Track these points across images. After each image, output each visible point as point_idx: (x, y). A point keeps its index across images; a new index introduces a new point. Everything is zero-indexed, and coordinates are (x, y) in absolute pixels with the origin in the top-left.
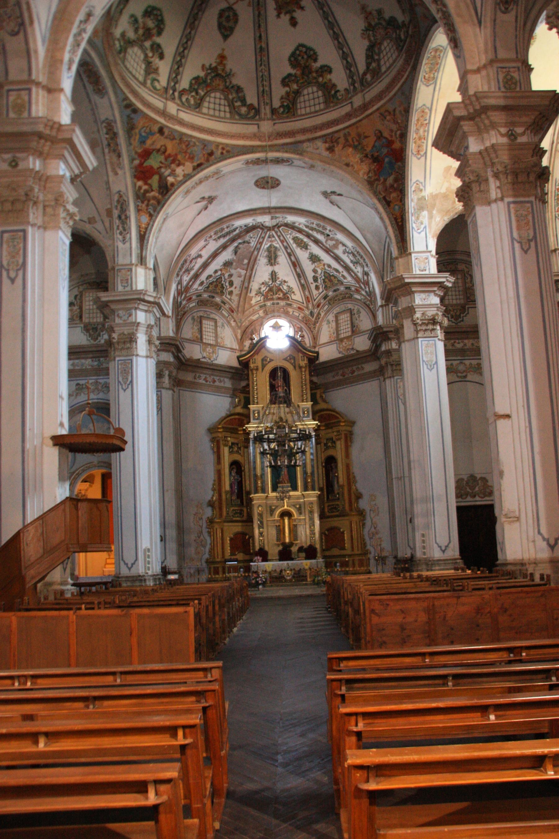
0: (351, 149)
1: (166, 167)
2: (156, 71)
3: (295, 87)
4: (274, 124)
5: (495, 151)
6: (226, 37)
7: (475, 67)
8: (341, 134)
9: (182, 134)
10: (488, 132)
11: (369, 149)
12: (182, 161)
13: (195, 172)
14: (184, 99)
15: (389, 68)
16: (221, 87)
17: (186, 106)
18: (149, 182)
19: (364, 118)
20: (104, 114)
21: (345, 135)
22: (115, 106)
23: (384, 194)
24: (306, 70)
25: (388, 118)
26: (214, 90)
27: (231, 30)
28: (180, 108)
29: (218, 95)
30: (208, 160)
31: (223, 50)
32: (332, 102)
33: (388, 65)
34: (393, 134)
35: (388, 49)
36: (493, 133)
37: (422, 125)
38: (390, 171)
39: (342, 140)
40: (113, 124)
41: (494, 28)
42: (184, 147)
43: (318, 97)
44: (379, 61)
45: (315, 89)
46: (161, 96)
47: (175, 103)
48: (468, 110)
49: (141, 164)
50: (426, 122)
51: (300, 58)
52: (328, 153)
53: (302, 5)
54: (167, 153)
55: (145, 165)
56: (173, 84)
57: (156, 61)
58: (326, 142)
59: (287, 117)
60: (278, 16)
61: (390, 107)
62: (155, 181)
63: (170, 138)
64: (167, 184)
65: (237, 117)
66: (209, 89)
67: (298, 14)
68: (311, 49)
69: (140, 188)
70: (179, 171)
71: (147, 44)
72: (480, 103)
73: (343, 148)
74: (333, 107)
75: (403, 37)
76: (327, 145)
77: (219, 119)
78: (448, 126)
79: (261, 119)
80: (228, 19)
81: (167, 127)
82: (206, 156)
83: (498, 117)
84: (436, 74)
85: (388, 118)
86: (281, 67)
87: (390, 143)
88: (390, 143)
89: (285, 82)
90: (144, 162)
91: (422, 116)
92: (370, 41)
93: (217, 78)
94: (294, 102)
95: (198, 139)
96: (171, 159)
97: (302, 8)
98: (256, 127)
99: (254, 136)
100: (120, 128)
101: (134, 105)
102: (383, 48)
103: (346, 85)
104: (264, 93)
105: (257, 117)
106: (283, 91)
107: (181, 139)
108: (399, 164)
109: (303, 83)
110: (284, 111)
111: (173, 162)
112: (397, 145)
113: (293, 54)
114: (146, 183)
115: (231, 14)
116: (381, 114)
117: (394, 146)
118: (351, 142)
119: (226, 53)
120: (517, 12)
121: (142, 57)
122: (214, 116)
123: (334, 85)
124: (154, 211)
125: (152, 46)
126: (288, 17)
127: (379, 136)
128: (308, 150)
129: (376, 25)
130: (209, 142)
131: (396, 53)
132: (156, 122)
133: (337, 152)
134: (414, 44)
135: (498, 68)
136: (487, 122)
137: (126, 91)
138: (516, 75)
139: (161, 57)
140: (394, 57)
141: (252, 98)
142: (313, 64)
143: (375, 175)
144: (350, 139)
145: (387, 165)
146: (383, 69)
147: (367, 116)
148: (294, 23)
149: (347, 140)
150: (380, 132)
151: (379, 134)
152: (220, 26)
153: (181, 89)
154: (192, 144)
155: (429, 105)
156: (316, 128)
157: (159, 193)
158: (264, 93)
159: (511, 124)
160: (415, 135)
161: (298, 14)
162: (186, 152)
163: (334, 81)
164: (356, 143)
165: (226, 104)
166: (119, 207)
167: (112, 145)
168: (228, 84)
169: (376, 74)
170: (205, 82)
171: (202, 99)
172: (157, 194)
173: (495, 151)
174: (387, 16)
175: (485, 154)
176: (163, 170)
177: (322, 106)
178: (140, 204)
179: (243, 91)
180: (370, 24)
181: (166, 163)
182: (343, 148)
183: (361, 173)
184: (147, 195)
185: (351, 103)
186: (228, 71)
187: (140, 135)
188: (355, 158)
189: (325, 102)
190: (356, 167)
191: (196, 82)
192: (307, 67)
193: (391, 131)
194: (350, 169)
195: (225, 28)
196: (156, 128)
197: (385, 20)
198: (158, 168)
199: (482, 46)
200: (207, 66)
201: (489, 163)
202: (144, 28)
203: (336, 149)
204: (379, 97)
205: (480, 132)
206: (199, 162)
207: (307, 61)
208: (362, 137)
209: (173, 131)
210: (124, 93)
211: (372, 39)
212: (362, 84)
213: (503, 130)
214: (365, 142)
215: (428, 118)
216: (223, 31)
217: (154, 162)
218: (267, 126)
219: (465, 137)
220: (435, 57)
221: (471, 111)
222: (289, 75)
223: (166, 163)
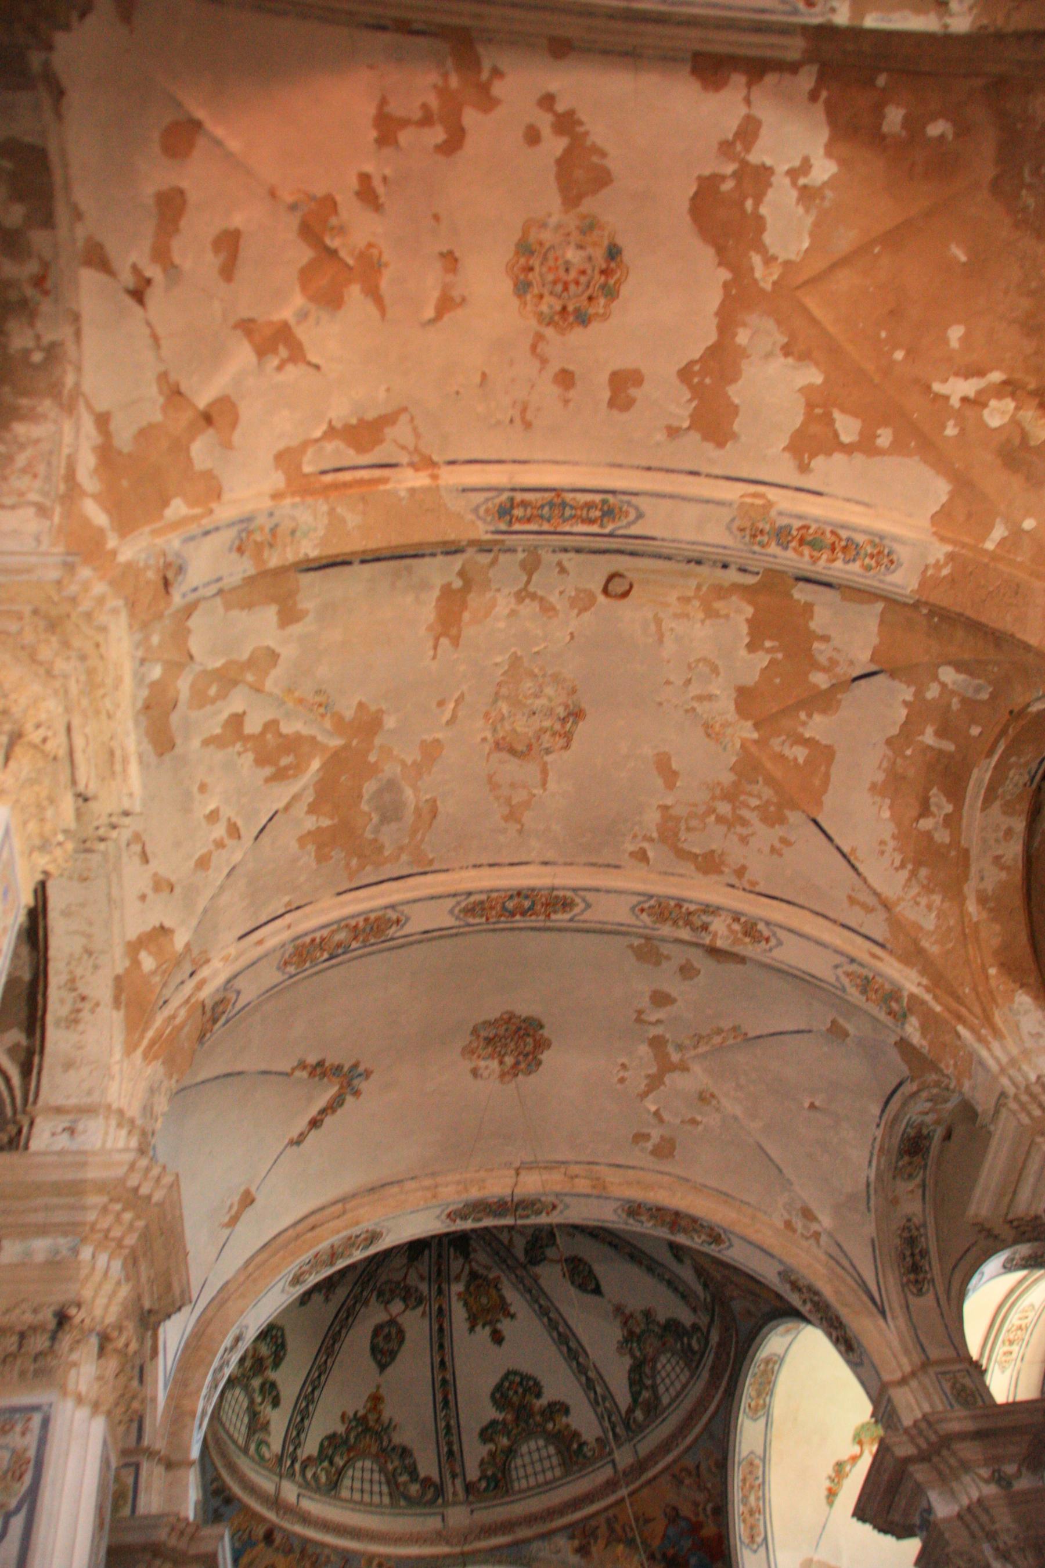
0: (620, 1548)
2: (265, 1427)
3: (505, 1441)
4: (472, 1512)
5: (986, 1510)
6: (382, 1367)
7: (898, 1375)
8: (602, 1519)
9: (306, 1541)
10: (958, 1479)
11: (656, 1544)
14: (309, 1474)
15: (677, 1396)
16: (374, 1449)
17: (313, 1487)
19: (642, 1486)
21: (608, 1521)
24: (522, 1412)
25: (687, 1481)
26: (363, 1455)
27: (393, 1355)
28: (303, 1491)
29: (368, 1464)
32: (576, 1463)
33: (673, 1392)
35: (668, 1367)
36: (967, 1479)
37: (752, 1487)
39: (603, 1530)
41: (910, 1317)
43: (549, 1457)
44: (654, 1388)
45: (541, 1443)
46: (271, 1470)
47: (293, 1481)
48: (918, 1446)
50: (757, 1482)
56: (291, 1448)
57: (267, 1411)
59: (495, 1498)
60: (472, 1329)
61: (689, 1462)
65: (402, 1503)
67: (505, 1326)
68: (529, 1378)
71: (256, 1383)
72: (936, 1432)
74: (580, 1470)
75: (696, 1346)
76: (576, 1543)
77: (368, 1507)
78: (886, 1477)
79: (446, 1504)
80: (388, 1338)
81: (281, 1528)
83: (969, 1451)
85: (687, 1481)
86: (477, 1408)
87: (695, 1528)
88: (695, 1528)
89: (487, 1434)
91: (751, 1473)
92: (633, 1356)
93: (368, 1434)
94: (505, 1469)
95: (335, 1549)
97: (513, 1316)
98: (439, 1518)
99: (439, 1537)
101: (230, 1489)
102: (659, 1366)
103: (598, 1432)
104: (451, 1455)
105: (440, 1501)
106: (483, 1450)
107: (303, 1551)
109: (520, 1434)
110: (488, 1485)
112: (709, 1530)
113: (499, 1387)
115: (394, 1331)
116: (674, 1476)
119: (383, 1392)
120: (936, 1294)
121: (246, 1404)
122: (361, 1502)
123: (576, 1435)
125: (263, 1386)
126: (488, 1330)
127: (674, 1515)
128: (542, 1554)
129: (643, 1332)
130: (355, 1553)
131: (687, 1373)
132: (263, 1519)
135: (937, 1374)
136: (953, 1461)
137: (219, 1464)
138: (967, 1381)
139: (276, 1403)
140: (683, 1378)
141: (427, 1466)
142: (535, 1401)
144: (618, 1527)
146: (665, 1400)
147: (649, 1482)
148: (497, 1338)
149: (611, 1530)
150: (675, 1509)
152: (374, 1349)
153: (305, 1456)
154: (323, 1559)
155: (759, 1451)
156: (551, 1513)
158: (451, 1455)
159: (994, 1460)
160: (741, 1508)
161: (505, 1326)
163: (574, 1426)
165: (383, 1479)
168: (385, 1443)
169: (653, 1409)
170: (346, 1441)
171: (340, 1473)
173: (986, 1510)
174: (661, 1318)
175: (968, 1518)
177: (558, 1472)
179: (411, 1455)
180: (631, 1333)
185: (613, 1462)
186: (386, 1421)
189: (563, 1464)
191: (330, 1444)
192: (525, 1407)
193: (696, 1504)
195: (382, 1352)
196: (260, 1531)
197: (658, 1324)
199: (896, 1343)
200: (351, 1414)
201: (980, 1534)
202: (253, 1356)
203: (594, 1549)
204: (665, 1447)
205: (945, 1479)
209: (288, 1535)
210: (216, 1469)
211: (638, 1354)
212: (627, 1427)
213: (985, 1472)
216: (379, 1357)
218: (458, 1516)
219: (919, 1490)
220: (765, 1372)
221: (924, 1445)
222: (493, 1423)
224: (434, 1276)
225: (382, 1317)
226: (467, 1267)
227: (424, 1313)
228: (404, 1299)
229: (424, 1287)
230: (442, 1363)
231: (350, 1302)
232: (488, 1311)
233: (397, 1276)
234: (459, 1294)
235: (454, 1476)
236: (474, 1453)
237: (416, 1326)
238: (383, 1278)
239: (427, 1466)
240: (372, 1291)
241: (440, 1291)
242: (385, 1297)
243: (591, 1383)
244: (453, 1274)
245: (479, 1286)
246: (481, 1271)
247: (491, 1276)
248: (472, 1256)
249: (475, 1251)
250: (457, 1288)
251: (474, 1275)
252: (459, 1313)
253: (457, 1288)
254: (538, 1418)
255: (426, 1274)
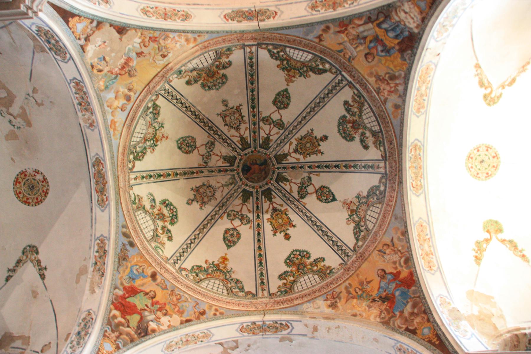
0: (355, 300)
1: (151, 312)
3: (292, 278)
12: (170, 312)
13: (182, 326)
18: (128, 317)
20: (101, 230)
21: (346, 288)
22: (113, 224)
23: (404, 327)
25: (387, 252)
26: (215, 278)
30: (198, 318)
31: (226, 254)
34: (397, 265)
37: (425, 240)
38: (405, 302)
39: (344, 294)
40: (106, 241)
42: (175, 299)
49: (123, 298)
50: (427, 237)
51: (295, 259)
52: (330, 309)
53: (294, 224)
54: (154, 300)
55: (128, 300)
58: (327, 300)
60: (275, 235)
62: (134, 319)
63: (161, 287)
64: (147, 329)
66: (209, 276)
67: (291, 231)
69: (115, 317)
70: (165, 320)
73: (347, 301)
76: (329, 302)
80: (232, 235)
82: (197, 314)
84: (422, 181)
86: (277, 265)
90: (128, 297)
91: (422, 231)
92: (354, 221)
96: (159, 306)
100: (111, 248)
104: (262, 281)
108: (413, 288)
111: (160, 309)
114: (123, 316)
115: (235, 233)
117: (402, 276)
118: (354, 293)
124: (124, 346)
126: (283, 234)
127: (383, 274)
128: (308, 310)
133: (340, 307)
134: (394, 164)
141: (250, 286)
142: (307, 260)
143: (388, 313)
144: (352, 290)
145: (399, 298)
148: (287, 237)
149: (349, 293)
150: (383, 270)
151: (383, 273)
154: (183, 298)
155: (425, 218)
157: (136, 332)
158: (262, 281)
161: (291, 231)
162: (175, 305)
164: (360, 293)
166: (82, 325)
167: (98, 263)
172: (133, 333)
176: (146, 313)
178: (109, 331)
181: (152, 308)
182: (347, 301)
183: (372, 318)
184: (121, 327)
187: (131, 271)
188: (360, 306)
190: (364, 314)
193: (395, 263)
194: (358, 318)
195: (229, 241)
198: (141, 310)
206: (188, 318)
207: (301, 260)
208: (365, 283)
214: (369, 288)
215: (428, 232)
216: (227, 242)
217: (139, 301)
222: (285, 272)
223: (152, 308)
224: (255, 209)
225: (230, 226)
226: (271, 206)
227: (251, 227)
228: (241, 220)
229: (250, 216)
230: (259, 248)
231: (213, 213)
232: (282, 226)
233: (238, 209)
234: (268, 219)
235: (263, 290)
236: (275, 284)
237: (247, 232)
238: (230, 208)
239: (250, 286)
240: (224, 213)
241: (258, 216)
242: (232, 216)
243: (336, 245)
244: (265, 210)
245: (277, 215)
246: (278, 207)
247: (283, 209)
248: (273, 200)
249: (275, 197)
250: (267, 216)
251: (275, 210)
252: (268, 228)
253: (267, 216)
254: (309, 267)
255: (252, 210)
